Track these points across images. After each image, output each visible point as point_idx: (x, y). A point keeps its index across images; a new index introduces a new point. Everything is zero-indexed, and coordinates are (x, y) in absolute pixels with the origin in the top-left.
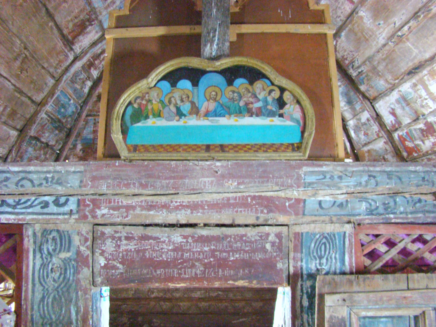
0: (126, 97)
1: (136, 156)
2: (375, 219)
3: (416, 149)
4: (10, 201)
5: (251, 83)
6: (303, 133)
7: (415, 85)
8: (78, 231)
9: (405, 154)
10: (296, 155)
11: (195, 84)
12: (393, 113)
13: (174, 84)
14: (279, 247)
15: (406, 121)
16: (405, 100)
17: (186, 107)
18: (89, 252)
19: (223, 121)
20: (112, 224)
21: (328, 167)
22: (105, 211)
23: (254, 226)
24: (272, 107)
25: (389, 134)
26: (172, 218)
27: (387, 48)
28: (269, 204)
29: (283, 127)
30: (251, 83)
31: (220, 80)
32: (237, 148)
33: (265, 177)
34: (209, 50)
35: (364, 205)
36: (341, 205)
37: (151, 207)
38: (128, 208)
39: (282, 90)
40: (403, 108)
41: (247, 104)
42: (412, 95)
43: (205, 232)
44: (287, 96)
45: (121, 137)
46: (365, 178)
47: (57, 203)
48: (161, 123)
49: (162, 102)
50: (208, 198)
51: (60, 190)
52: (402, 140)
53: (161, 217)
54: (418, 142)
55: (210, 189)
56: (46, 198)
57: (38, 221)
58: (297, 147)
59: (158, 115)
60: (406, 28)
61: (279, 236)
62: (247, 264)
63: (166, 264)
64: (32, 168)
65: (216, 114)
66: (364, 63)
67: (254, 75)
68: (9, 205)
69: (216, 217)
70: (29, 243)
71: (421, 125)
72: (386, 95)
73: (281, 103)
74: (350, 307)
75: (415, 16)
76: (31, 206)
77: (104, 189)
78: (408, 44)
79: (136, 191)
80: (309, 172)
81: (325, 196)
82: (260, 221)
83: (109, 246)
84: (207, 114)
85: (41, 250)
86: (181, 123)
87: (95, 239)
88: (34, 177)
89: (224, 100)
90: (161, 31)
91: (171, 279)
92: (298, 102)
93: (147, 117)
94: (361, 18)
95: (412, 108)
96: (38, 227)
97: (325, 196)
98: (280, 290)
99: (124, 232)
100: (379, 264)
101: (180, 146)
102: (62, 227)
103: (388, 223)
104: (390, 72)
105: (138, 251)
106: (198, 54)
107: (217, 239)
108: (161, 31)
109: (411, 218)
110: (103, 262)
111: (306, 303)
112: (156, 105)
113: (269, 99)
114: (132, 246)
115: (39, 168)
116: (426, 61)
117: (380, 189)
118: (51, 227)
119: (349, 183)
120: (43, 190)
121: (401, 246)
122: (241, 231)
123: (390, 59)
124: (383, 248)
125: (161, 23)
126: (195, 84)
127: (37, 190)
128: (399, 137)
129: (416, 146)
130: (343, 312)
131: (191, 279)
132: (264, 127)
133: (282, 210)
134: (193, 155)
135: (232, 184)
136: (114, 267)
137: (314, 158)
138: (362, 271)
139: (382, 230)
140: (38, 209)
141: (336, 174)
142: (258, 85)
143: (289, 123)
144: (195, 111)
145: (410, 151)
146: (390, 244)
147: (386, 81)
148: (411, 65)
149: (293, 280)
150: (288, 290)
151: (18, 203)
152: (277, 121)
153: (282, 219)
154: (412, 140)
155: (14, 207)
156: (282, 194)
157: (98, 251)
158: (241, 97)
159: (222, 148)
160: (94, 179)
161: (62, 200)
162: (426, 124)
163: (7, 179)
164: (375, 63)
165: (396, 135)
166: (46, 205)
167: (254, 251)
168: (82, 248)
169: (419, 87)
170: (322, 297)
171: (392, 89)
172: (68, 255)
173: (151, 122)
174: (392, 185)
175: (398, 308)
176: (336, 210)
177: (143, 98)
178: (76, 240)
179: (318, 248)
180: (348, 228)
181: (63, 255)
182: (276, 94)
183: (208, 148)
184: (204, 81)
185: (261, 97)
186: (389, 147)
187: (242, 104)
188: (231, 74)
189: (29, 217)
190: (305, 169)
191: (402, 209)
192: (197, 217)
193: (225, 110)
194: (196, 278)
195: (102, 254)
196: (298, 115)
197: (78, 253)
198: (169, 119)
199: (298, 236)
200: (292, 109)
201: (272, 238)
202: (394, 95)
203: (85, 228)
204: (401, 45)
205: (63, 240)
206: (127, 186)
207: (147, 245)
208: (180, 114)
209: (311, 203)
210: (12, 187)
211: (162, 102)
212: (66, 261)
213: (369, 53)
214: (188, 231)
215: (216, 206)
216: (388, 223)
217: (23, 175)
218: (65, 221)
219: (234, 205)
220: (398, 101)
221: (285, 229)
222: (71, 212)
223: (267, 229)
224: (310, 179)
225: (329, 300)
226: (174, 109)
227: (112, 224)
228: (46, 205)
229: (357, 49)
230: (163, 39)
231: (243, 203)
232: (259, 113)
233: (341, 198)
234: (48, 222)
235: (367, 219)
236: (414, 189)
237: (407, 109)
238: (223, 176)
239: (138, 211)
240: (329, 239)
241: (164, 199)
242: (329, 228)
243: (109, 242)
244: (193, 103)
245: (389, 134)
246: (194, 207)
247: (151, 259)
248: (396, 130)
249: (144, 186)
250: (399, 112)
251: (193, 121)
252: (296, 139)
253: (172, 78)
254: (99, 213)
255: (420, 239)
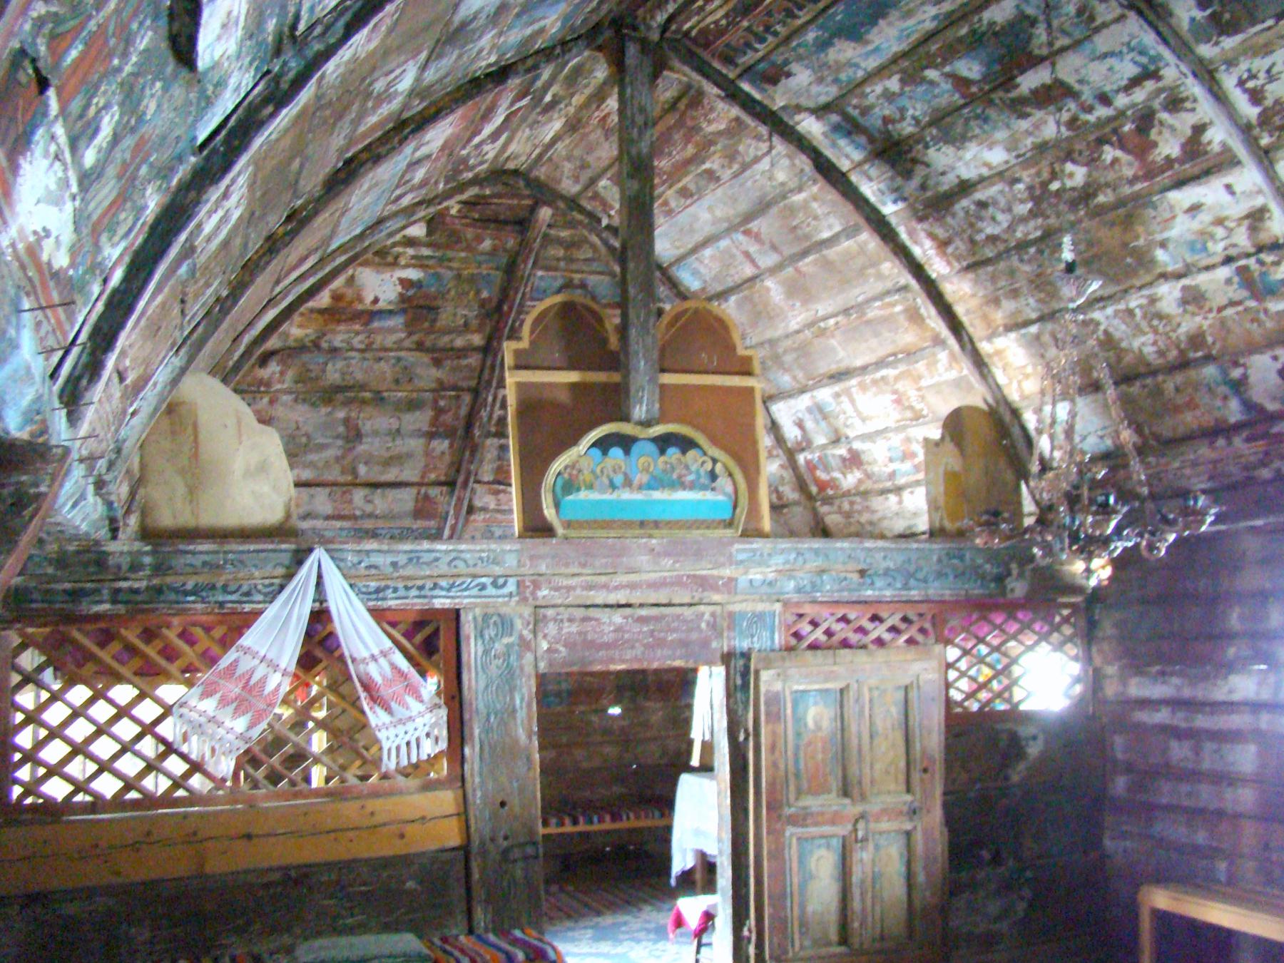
0: (558, 465)
1: (572, 533)
2: (802, 597)
3: (832, 483)
4: (443, 583)
5: (684, 452)
6: (735, 507)
7: (837, 395)
8: (521, 615)
9: (814, 490)
10: (729, 532)
11: (627, 452)
12: (800, 424)
13: (605, 453)
14: (713, 626)
15: (820, 440)
16: (820, 411)
17: (619, 479)
18: (530, 636)
19: (657, 495)
20: (554, 606)
21: (758, 544)
22: (545, 592)
23: (691, 605)
24: (705, 480)
25: (791, 454)
26: (612, 598)
27: (801, 336)
28: (704, 583)
29: (714, 501)
30: (684, 452)
31: (652, 448)
32: (671, 524)
33: (698, 554)
34: (639, 412)
35: (792, 584)
36: (770, 584)
37: (590, 587)
38: (570, 589)
39: (715, 461)
40: (817, 422)
41: (680, 477)
42: (832, 406)
43: (644, 612)
44: (719, 467)
45: (553, 511)
46: (793, 556)
47: (494, 584)
48: (594, 496)
49: (593, 472)
50: (645, 577)
51: (497, 570)
52: (811, 466)
53: (600, 597)
54: (837, 475)
55: (647, 569)
56: (483, 580)
57: (476, 605)
58: (730, 524)
59: (590, 487)
60: (832, 322)
61: (713, 615)
62: (684, 644)
63: (607, 646)
64: (463, 547)
65: (650, 487)
66: (762, 344)
67: (686, 444)
68: (442, 588)
69: (653, 597)
70: (468, 628)
71: (842, 451)
72: (790, 396)
73: (713, 476)
74: (784, 681)
75: (846, 311)
76: (467, 589)
77: (543, 569)
78: (833, 342)
79: (576, 570)
80: (741, 549)
81: (756, 575)
82: (696, 600)
83: (551, 629)
84: (640, 488)
85: (482, 636)
86: (614, 496)
87: (537, 622)
88: (468, 556)
89: (657, 473)
90: (573, 377)
91: (612, 660)
92: (730, 475)
93: (579, 490)
94: (768, 290)
95: (829, 424)
96: (478, 611)
97: (756, 575)
98: (703, 672)
99: (565, 613)
100: (805, 644)
101: (614, 522)
102: (503, 610)
103: (814, 602)
104: (802, 368)
105: (580, 633)
106: (626, 418)
107: (657, 619)
108: (573, 377)
109: (836, 596)
110: (545, 645)
111: (739, 682)
112: (587, 476)
113: (702, 471)
114: (574, 628)
115: (471, 547)
116: (855, 369)
117: (808, 566)
118: (491, 611)
119: (778, 560)
120: (478, 570)
121: (824, 626)
122: (678, 610)
123: (803, 351)
124: (809, 628)
125: (572, 367)
126: (627, 452)
127: (472, 570)
128: (808, 462)
129: (833, 480)
130: (778, 686)
131: (631, 660)
132: (699, 502)
133: (716, 589)
134: (629, 533)
135: (667, 562)
136: (557, 651)
137: (745, 534)
138: (790, 649)
139: (808, 609)
140: (475, 592)
141: (766, 552)
142: (692, 453)
143: (721, 498)
144: (628, 483)
145: (822, 486)
146: (814, 624)
147: (794, 378)
148: (834, 368)
149: (727, 658)
150: (720, 671)
151: (452, 586)
152: (709, 495)
153: (716, 598)
154: (827, 469)
155: (448, 590)
156: (715, 572)
157: (540, 635)
158: (673, 469)
159: (657, 524)
160: (532, 558)
161: (501, 581)
162: (850, 450)
163: (437, 559)
164: (780, 350)
165: (801, 459)
166: (483, 587)
167: (690, 630)
168: (525, 632)
169: (844, 399)
170: (757, 672)
171: (803, 391)
172: (511, 640)
173: (583, 495)
174: (819, 563)
175: (826, 681)
176: (765, 589)
177: (573, 466)
178: (518, 624)
179: (749, 627)
180: (778, 607)
181: (506, 640)
182: (709, 466)
183: (642, 524)
184: (636, 449)
185: (693, 468)
186: (787, 475)
187: (675, 476)
188: (663, 443)
189: (466, 601)
190: (737, 546)
191: (828, 588)
192: (636, 597)
193: (657, 483)
194: (636, 659)
195: (545, 636)
196: (729, 489)
197: (521, 637)
198: (602, 491)
199: (731, 615)
200: (724, 482)
201: (707, 617)
202: (804, 401)
203: (527, 611)
204: (821, 340)
205: (505, 625)
206: (567, 565)
207: (588, 626)
208: (613, 487)
209: (743, 582)
210: (443, 568)
211: (593, 472)
212: (508, 646)
213: (770, 334)
214: (628, 611)
215: (654, 585)
216: (814, 602)
217: (453, 555)
218: (506, 604)
219: (672, 584)
220: (809, 410)
221: (718, 608)
222: (511, 595)
223: (702, 608)
224: (741, 557)
225: (765, 676)
226: (606, 481)
227: (554, 606)
228: (483, 587)
229: (754, 325)
230: (573, 387)
231: (678, 582)
232: (691, 486)
233: (771, 576)
234: (486, 605)
235: (795, 597)
236: (840, 567)
237: (823, 424)
238: (659, 554)
239: (578, 591)
240: (759, 617)
241: (603, 579)
242: (760, 607)
243: (551, 625)
244: (625, 474)
245: (791, 454)
246: (633, 586)
247: (592, 642)
248: (803, 450)
249: (584, 565)
250: (809, 425)
251: (626, 495)
252: (727, 515)
253: (603, 445)
254: (541, 594)
255: (844, 619)
